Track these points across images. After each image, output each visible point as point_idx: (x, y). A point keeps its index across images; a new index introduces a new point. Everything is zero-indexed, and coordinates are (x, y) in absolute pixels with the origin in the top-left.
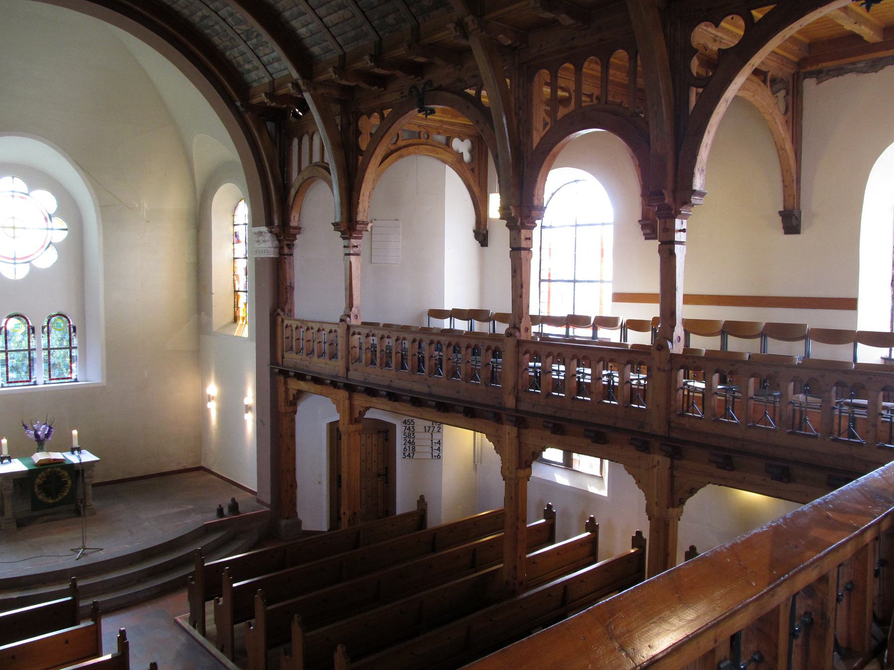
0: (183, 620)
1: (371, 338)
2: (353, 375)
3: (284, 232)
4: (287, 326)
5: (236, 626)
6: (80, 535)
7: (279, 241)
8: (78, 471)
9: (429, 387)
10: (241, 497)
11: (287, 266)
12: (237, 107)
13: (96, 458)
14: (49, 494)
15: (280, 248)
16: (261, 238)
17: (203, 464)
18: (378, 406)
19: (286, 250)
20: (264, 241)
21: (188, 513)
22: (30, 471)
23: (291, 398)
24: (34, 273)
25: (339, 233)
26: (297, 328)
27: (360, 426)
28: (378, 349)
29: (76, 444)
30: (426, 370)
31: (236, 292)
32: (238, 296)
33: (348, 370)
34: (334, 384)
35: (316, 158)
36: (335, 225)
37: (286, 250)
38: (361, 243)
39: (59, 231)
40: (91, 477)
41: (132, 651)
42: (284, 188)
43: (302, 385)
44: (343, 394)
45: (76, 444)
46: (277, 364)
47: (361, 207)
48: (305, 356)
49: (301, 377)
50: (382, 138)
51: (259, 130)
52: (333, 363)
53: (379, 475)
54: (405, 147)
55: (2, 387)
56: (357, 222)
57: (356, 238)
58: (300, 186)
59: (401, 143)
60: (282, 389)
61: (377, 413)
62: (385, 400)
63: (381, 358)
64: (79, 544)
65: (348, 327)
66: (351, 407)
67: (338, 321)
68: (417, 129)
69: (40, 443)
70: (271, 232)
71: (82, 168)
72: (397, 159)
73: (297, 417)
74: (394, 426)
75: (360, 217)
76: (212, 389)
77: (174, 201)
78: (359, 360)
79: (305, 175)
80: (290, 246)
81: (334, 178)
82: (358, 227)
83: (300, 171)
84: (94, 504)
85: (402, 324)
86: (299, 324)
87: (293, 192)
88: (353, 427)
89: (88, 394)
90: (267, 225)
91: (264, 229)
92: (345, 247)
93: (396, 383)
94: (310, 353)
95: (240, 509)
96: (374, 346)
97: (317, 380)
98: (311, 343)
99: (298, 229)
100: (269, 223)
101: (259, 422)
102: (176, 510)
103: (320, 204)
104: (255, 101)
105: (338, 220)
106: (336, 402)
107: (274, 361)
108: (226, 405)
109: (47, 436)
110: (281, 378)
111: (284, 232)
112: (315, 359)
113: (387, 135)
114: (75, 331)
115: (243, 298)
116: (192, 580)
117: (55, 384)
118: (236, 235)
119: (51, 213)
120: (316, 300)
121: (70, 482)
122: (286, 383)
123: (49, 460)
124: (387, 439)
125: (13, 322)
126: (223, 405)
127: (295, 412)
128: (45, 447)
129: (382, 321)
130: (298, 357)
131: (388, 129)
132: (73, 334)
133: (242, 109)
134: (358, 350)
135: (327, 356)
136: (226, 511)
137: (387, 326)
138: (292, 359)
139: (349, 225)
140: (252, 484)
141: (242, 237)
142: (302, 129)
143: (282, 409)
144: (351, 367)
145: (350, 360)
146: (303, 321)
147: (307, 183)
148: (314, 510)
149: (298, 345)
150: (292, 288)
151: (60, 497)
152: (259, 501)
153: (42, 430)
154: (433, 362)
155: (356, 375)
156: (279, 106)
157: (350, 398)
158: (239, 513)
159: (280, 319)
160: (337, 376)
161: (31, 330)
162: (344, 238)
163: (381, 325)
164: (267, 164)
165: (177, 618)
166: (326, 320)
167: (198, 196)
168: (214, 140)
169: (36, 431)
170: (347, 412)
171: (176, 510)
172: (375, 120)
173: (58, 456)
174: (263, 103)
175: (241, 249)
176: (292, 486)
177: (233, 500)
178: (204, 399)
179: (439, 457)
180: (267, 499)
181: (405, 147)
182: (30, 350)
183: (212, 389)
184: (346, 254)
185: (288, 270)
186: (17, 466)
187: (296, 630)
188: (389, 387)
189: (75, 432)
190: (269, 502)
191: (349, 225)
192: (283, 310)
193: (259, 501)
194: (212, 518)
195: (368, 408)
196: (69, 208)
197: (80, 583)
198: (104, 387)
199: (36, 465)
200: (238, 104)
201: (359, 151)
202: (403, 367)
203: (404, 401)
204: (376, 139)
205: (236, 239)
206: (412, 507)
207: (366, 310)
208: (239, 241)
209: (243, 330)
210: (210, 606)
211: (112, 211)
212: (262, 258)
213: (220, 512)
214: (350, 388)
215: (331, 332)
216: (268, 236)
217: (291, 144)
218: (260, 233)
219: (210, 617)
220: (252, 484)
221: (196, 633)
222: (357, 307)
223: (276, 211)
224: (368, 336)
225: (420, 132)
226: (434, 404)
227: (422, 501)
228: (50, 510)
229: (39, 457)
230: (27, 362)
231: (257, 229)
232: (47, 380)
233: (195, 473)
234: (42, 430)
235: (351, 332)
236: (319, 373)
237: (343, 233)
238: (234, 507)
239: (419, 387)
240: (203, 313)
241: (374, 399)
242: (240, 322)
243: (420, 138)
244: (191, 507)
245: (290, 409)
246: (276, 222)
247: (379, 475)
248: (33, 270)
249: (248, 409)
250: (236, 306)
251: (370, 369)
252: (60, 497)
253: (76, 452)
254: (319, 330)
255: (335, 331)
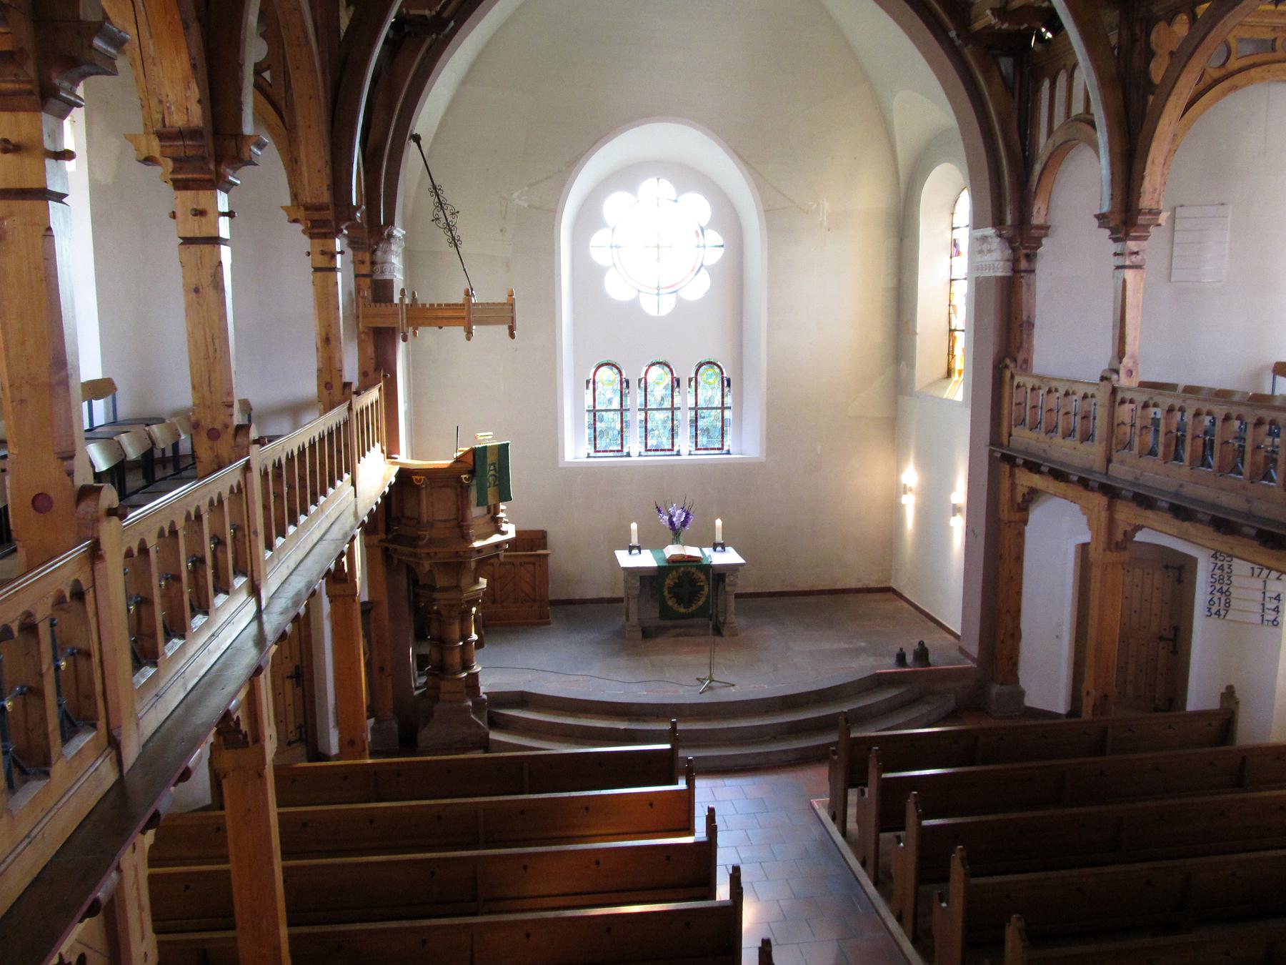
0: (821, 805)
1: (1152, 410)
2: (1115, 469)
3: (1021, 235)
4: (1018, 386)
5: (882, 835)
6: (707, 661)
7: (1014, 249)
8: (720, 575)
9: (1249, 501)
10: (934, 642)
11: (1024, 289)
12: (951, 41)
13: (741, 561)
14: (680, 601)
15: (1015, 261)
16: (985, 247)
17: (893, 584)
18: (1156, 525)
19: (1023, 264)
20: (990, 251)
21: (856, 653)
22: (659, 567)
23: (1019, 499)
24: (681, 306)
25: (1107, 232)
26: (1033, 389)
27: (1125, 556)
28: (1162, 429)
29: (634, 541)
30: (1246, 470)
31: (951, 331)
32: (954, 338)
33: (1109, 461)
34: (1084, 483)
35: (1078, 108)
36: (1101, 218)
37: (1023, 264)
38: (1151, 247)
39: (714, 250)
40: (735, 585)
41: (721, 840)
42: (1023, 161)
43: (1037, 481)
44: (1099, 500)
45: (719, 538)
46: (1001, 445)
47: (1147, 185)
48: (1043, 434)
49: (1033, 467)
50: (1192, 54)
51: (986, 73)
52: (1086, 447)
53: (1161, 638)
54: (1240, 70)
55: (589, 456)
56: (1139, 212)
57: (1136, 238)
58: (1050, 158)
59: (1233, 64)
60: (1006, 484)
61: (1157, 534)
62: (1169, 517)
63: (1167, 446)
64: (704, 673)
65: (1114, 391)
66: (1111, 522)
67: (1097, 380)
68: (1269, 36)
69: (676, 533)
70: (1000, 236)
71: (740, 157)
72: (1224, 94)
73: (1029, 530)
74: (1193, 561)
75: (1145, 202)
76: (910, 476)
77: (867, 197)
78: (1128, 445)
79: (1058, 138)
80: (1031, 258)
81: (1102, 137)
82: (1141, 220)
83: (1050, 131)
84: (736, 620)
85: (1219, 386)
86: (1037, 383)
87: (1038, 168)
88: (1113, 557)
89: (745, 470)
90: (994, 226)
91: (990, 231)
92: (1116, 254)
93: (1191, 490)
94: (1051, 430)
95: (931, 658)
96: (1156, 422)
97: (1058, 475)
98: (1054, 414)
99: (1045, 228)
100: (998, 222)
101: (970, 532)
102: (843, 645)
103: (1083, 183)
104: (978, 26)
105: (1105, 209)
106: (1086, 511)
107: (995, 440)
108: (924, 500)
109: (684, 523)
110: (1006, 467)
111: (1021, 235)
112: (1058, 439)
113: (1200, 49)
114: (729, 385)
115: (961, 339)
116: (834, 753)
117: (703, 456)
118: (955, 244)
119: (703, 225)
120: (1067, 346)
121: (706, 588)
122: (1012, 475)
123: (683, 556)
124: (1179, 581)
125: (656, 372)
126: (920, 500)
127: (1025, 522)
128: (681, 538)
129: (1182, 380)
130: (1033, 435)
131: (1202, 40)
132: (726, 390)
133: (958, 42)
134: (1128, 429)
135: (1078, 435)
136: (909, 658)
137: (1191, 390)
138: (1024, 438)
139: (1126, 217)
140: (954, 623)
141: (964, 246)
142: (1052, 62)
143: (1005, 515)
144: (1116, 457)
145: (1115, 443)
146: (1042, 378)
147: (1060, 152)
148: (1046, 678)
149: (1034, 415)
150: (1031, 325)
151: (694, 607)
152: (961, 650)
153: (678, 517)
154: (1261, 456)
155: (1124, 470)
156: (1016, 28)
157: (1110, 508)
158: (929, 664)
159: (1008, 375)
160: (1090, 471)
161: (676, 383)
162: (1115, 240)
163: (1180, 389)
164: (997, 127)
165: (814, 802)
166: (1077, 378)
167: (902, 186)
168: (922, 100)
169: (671, 517)
170: (1103, 531)
171: (843, 645)
172: (1181, 28)
173: (693, 551)
174: (990, 27)
175: (961, 266)
176: (1013, 635)
177: (921, 644)
178: (900, 490)
179: (1275, 623)
180: (974, 649)
181: (1240, 70)
182: (673, 409)
183: (910, 476)
184: (1118, 267)
185: (1024, 296)
186: (646, 560)
187: (957, 870)
188: (1176, 495)
189: (719, 523)
190: (976, 656)
191: (1126, 217)
192: (1015, 360)
193: (961, 650)
194: (888, 665)
195: (1140, 528)
196: (728, 219)
197: (680, 727)
198: (762, 465)
199: (668, 561)
200: (953, 34)
201: (1149, 86)
202: (1205, 463)
203: (1200, 521)
204: (1181, 58)
205: (954, 251)
206: (1213, 703)
207: (1153, 359)
208: (958, 254)
209: (957, 391)
210: (853, 795)
211: (779, 216)
212: (986, 278)
213: (901, 659)
214: (1110, 492)
215: (1085, 397)
216: (995, 243)
217: (1038, 90)
218: (984, 239)
219: (852, 812)
220: (954, 623)
221: (834, 829)
222: (1132, 357)
223: (1012, 207)
224: (1146, 406)
225: (1274, 40)
226: (1253, 532)
227: (1229, 694)
228: (683, 622)
229: (672, 550)
230: (720, 424)
231: (980, 233)
232: (643, 449)
233: (878, 596)
234: (678, 517)
235: (1118, 398)
236: (1063, 464)
237: (1114, 231)
238: (922, 654)
239: (1231, 501)
240: (903, 363)
241: (1149, 513)
242: (956, 377)
243: (1274, 50)
244: (863, 644)
245: (1017, 516)
246: (1009, 220)
247: (1161, 638)
248: (680, 301)
249: (956, 510)
250: (951, 353)
251: (1147, 462)
252: (694, 607)
253: (719, 549)
254: (1067, 394)
255: (1093, 396)
